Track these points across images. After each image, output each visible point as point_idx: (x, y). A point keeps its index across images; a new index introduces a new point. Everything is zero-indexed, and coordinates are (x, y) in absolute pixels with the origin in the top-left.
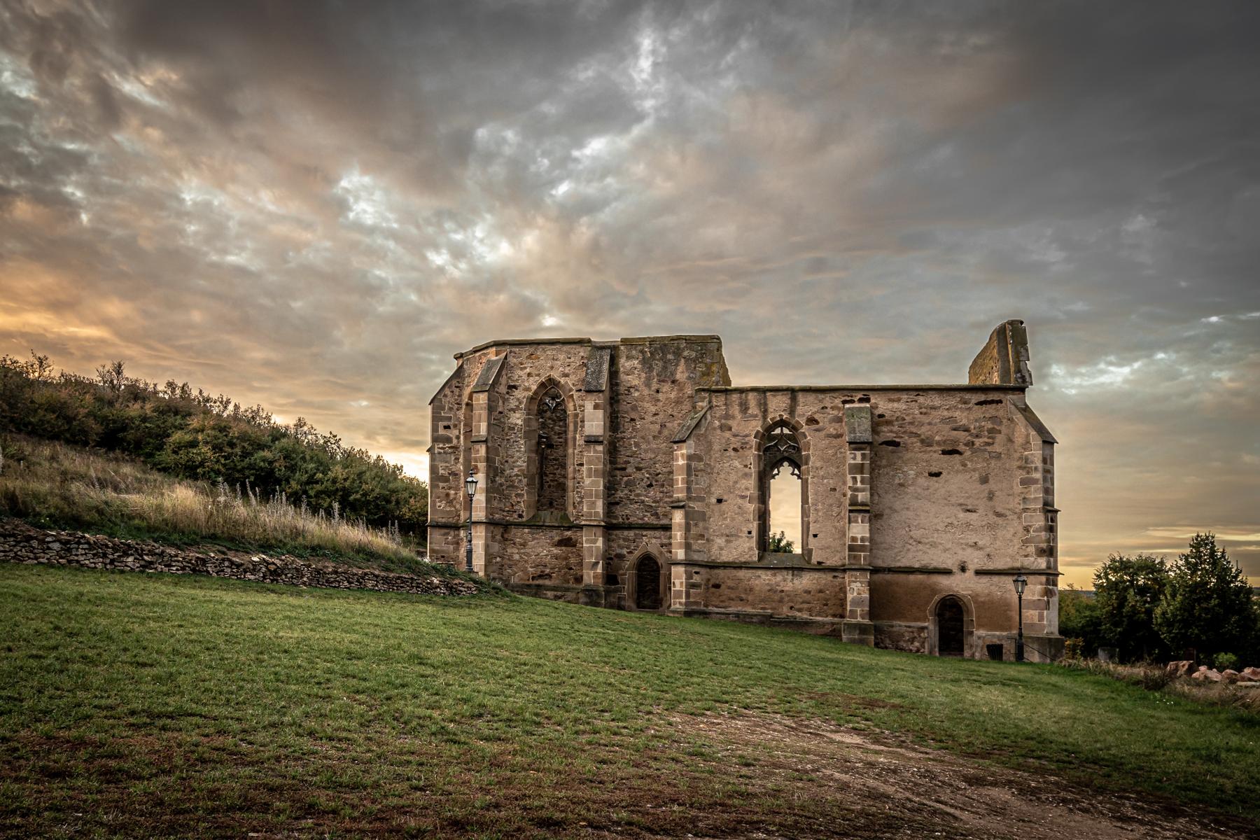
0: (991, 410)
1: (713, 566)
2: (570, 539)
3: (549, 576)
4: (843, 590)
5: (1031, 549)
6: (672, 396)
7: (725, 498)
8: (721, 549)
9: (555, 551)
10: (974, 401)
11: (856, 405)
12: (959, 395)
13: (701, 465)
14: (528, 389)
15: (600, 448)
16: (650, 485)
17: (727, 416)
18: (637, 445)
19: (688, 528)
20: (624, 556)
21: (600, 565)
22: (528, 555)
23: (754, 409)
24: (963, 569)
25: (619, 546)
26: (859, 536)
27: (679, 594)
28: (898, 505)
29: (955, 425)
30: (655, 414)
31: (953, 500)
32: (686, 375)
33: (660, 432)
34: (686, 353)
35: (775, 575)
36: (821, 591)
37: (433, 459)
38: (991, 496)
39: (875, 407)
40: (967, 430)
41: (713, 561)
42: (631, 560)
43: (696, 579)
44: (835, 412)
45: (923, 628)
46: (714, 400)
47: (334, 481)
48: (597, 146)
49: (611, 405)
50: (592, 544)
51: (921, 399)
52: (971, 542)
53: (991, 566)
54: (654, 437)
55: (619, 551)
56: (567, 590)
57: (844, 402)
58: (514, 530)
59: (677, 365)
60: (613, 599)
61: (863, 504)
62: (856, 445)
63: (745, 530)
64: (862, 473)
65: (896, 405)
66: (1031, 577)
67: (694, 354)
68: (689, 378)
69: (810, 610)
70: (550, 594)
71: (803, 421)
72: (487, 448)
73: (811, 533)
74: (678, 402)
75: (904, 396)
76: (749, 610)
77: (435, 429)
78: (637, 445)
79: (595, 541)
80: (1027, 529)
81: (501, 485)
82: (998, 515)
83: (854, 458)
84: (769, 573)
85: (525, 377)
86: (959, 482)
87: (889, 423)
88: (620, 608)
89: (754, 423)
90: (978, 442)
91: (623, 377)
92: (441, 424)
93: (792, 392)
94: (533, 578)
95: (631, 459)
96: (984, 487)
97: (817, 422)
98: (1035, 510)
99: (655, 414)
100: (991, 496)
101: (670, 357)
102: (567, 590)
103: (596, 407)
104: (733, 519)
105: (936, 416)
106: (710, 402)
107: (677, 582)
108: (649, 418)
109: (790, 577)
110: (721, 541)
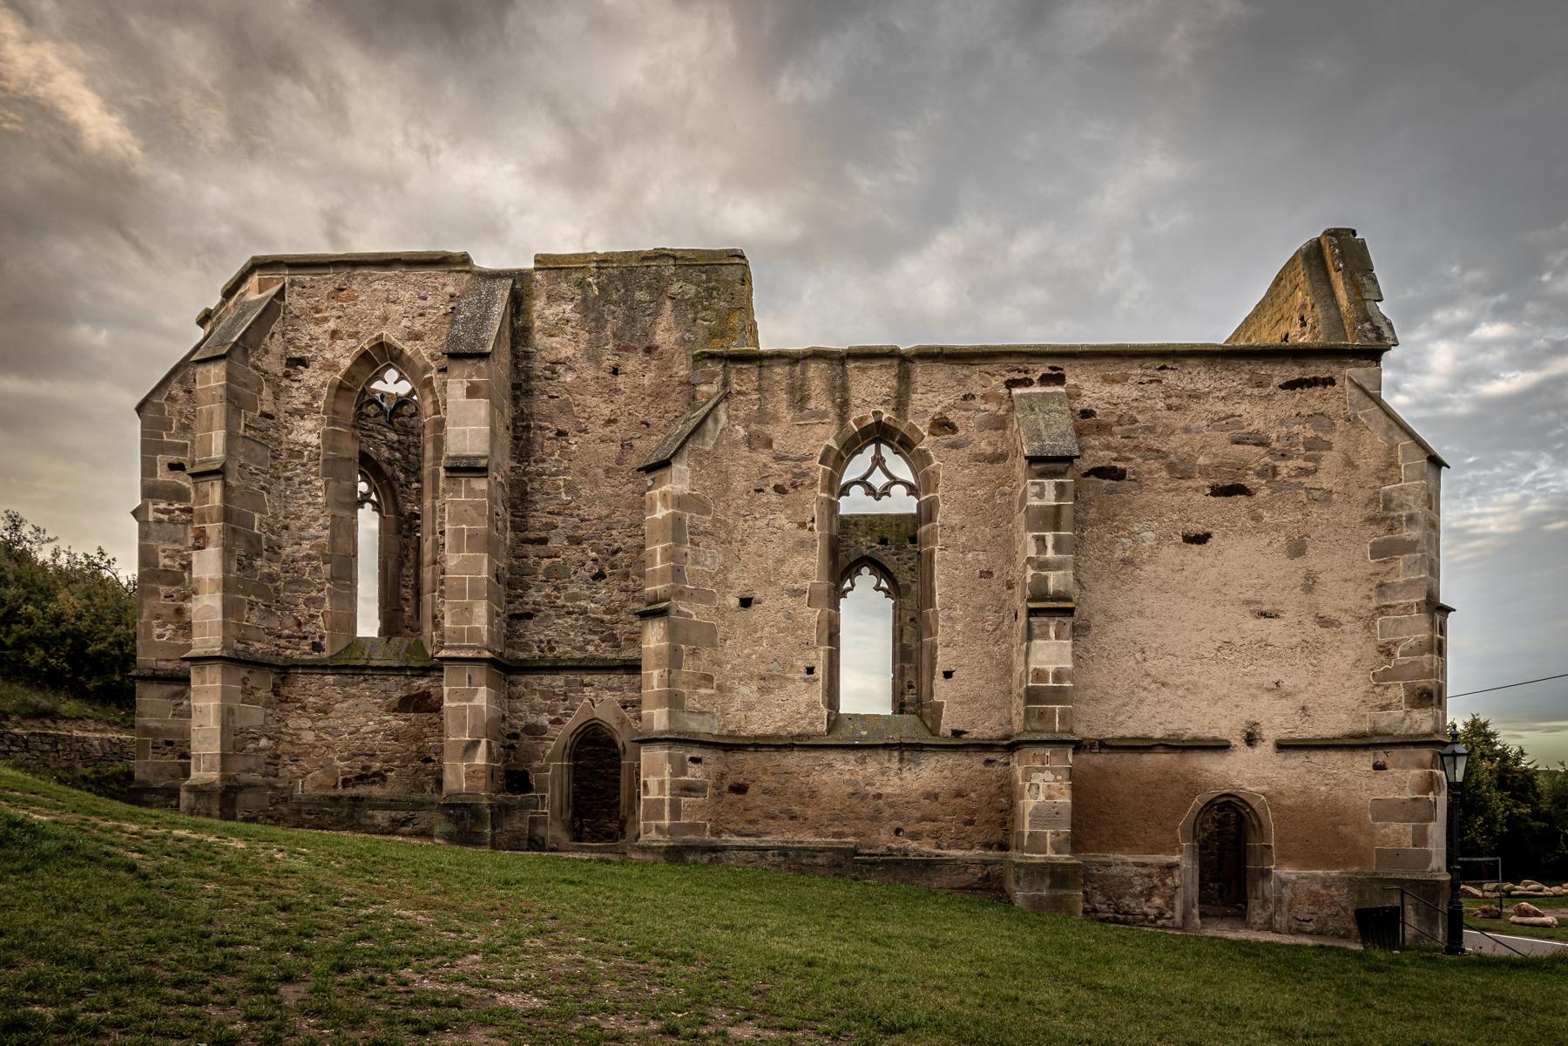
0: (1311, 399)
1: (729, 746)
2: (425, 695)
3: (381, 777)
4: (1007, 793)
5: (1398, 692)
6: (646, 381)
7: (758, 595)
8: (749, 707)
9: (395, 722)
10: (1277, 381)
11: (1037, 389)
12: (1246, 369)
13: (706, 522)
14: (331, 366)
15: (481, 484)
16: (600, 576)
17: (763, 416)
18: (571, 488)
19: (673, 659)
20: (544, 730)
21: (482, 749)
22: (334, 733)
23: (819, 401)
24: (1251, 739)
25: (532, 708)
26: (1051, 668)
27: (656, 809)
28: (1120, 605)
29: (1237, 433)
30: (610, 422)
31: (1232, 593)
32: (675, 336)
33: (619, 461)
34: (675, 288)
35: (863, 761)
36: (959, 794)
37: (144, 535)
38: (1310, 583)
39: (1074, 395)
40: (1262, 443)
41: (731, 735)
42: (559, 737)
43: (695, 774)
44: (992, 407)
45: (1171, 867)
46: (733, 379)
47: (58, 620)
48: (702, 691)
49: (515, 400)
50: (469, 702)
51: (1170, 377)
52: (1268, 681)
53: (1309, 731)
54: (608, 471)
55: (532, 719)
56: (420, 806)
57: (1011, 384)
58: (302, 680)
59: (656, 314)
60: (518, 823)
61: (1059, 597)
62: (1046, 464)
63: (801, 665)
64: (1056, 527)
65: (1117, 389)
66: (1396, 752)
67: (691, 290)
68: (682, 342)
69: (936, 835)
70: (381, 818)
71: (923, 429)
72: (226, 486)
73: (939, 670)
74: (658, 395)
75: (1136, 371)
76: (809, 839)
77: (148, 469)
78: (571, 488)
79: (471, 695)
80: (1386, 651)
81: (271, 578)
82: (1325, 622)
83: (1040, 495)
84: (851, 756)
85: (325, 340)
86: (1245, 556)
87: (1102, 428)
88: (536, 844)
89: (820, 430)
90: (1285, 468)
91: (539, 339)
92: (162, 460)
93: (902, 362)
94: (346, 783)
95: (559, 520)
96: (1298, 562)
97: (953, 429)
98: (1407, 609)
99: (610, 422)
100: (1310, 583)
101: (641, 295)
102: (420, 806)
103: (473, 392)
104: (774, 643)
105: (1199, 414)
106: (725, 384)
107: (653, 782)
108: (597, 430)
109: (895, 765)
110: (748, 691)
